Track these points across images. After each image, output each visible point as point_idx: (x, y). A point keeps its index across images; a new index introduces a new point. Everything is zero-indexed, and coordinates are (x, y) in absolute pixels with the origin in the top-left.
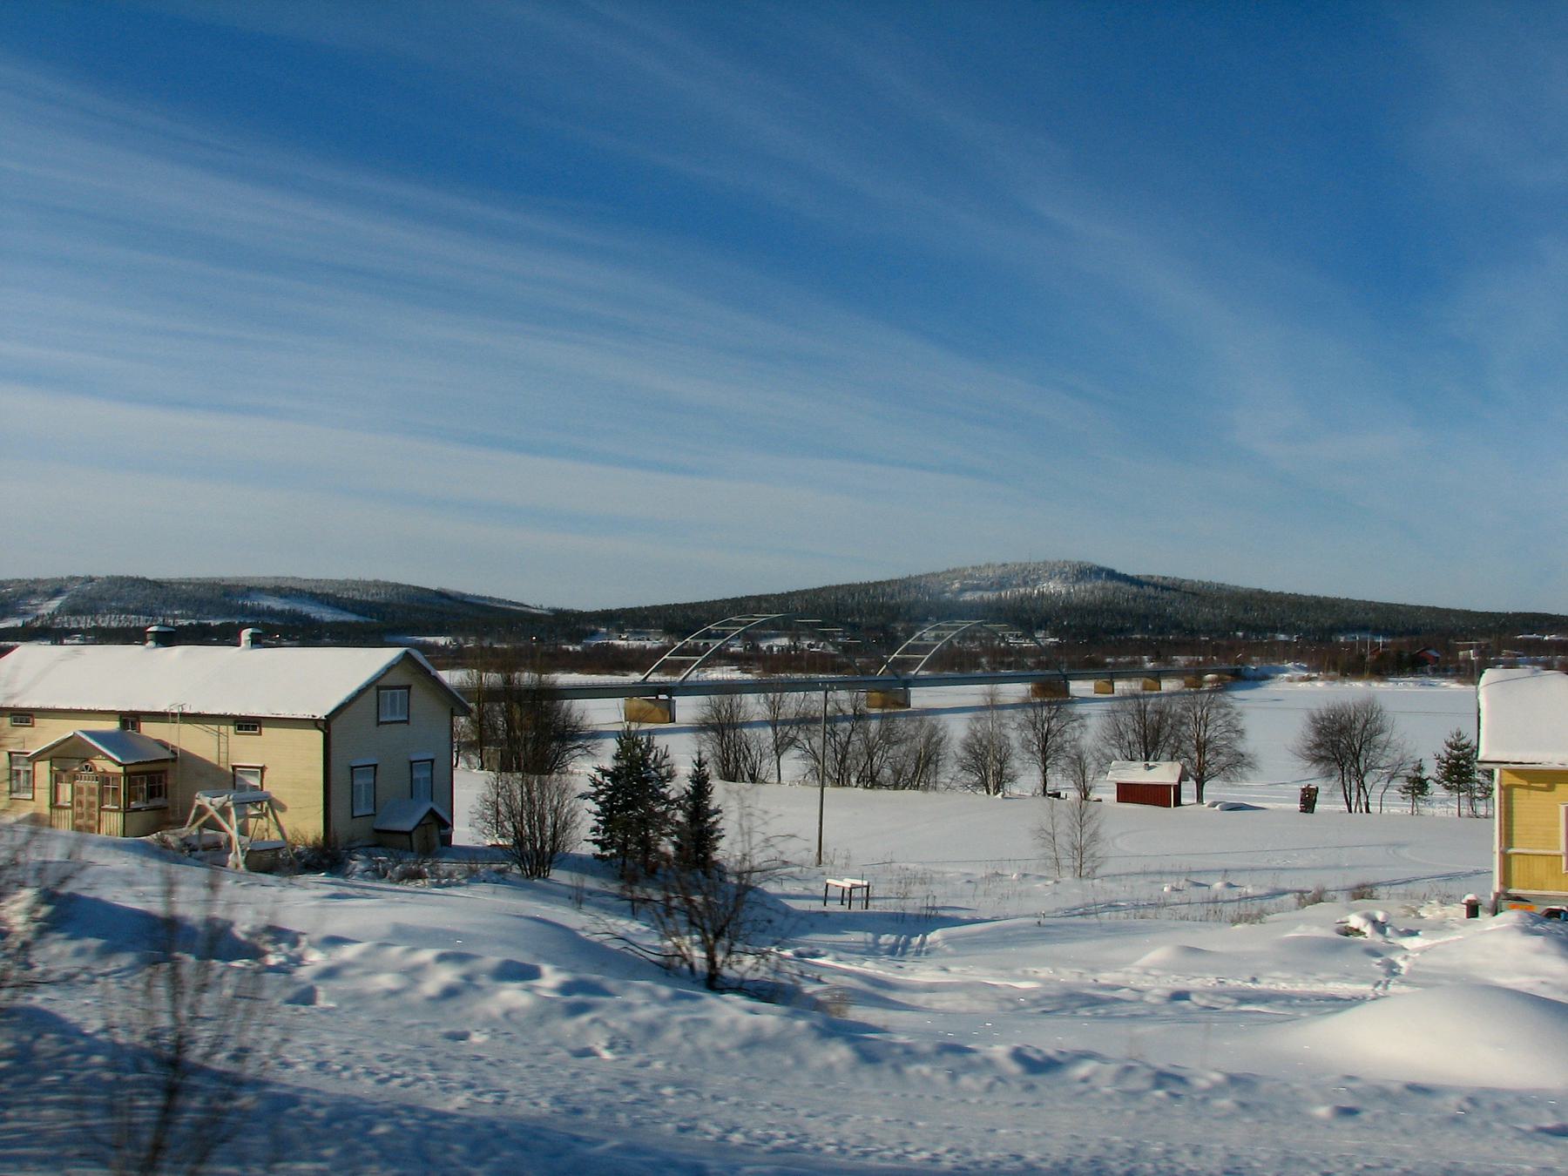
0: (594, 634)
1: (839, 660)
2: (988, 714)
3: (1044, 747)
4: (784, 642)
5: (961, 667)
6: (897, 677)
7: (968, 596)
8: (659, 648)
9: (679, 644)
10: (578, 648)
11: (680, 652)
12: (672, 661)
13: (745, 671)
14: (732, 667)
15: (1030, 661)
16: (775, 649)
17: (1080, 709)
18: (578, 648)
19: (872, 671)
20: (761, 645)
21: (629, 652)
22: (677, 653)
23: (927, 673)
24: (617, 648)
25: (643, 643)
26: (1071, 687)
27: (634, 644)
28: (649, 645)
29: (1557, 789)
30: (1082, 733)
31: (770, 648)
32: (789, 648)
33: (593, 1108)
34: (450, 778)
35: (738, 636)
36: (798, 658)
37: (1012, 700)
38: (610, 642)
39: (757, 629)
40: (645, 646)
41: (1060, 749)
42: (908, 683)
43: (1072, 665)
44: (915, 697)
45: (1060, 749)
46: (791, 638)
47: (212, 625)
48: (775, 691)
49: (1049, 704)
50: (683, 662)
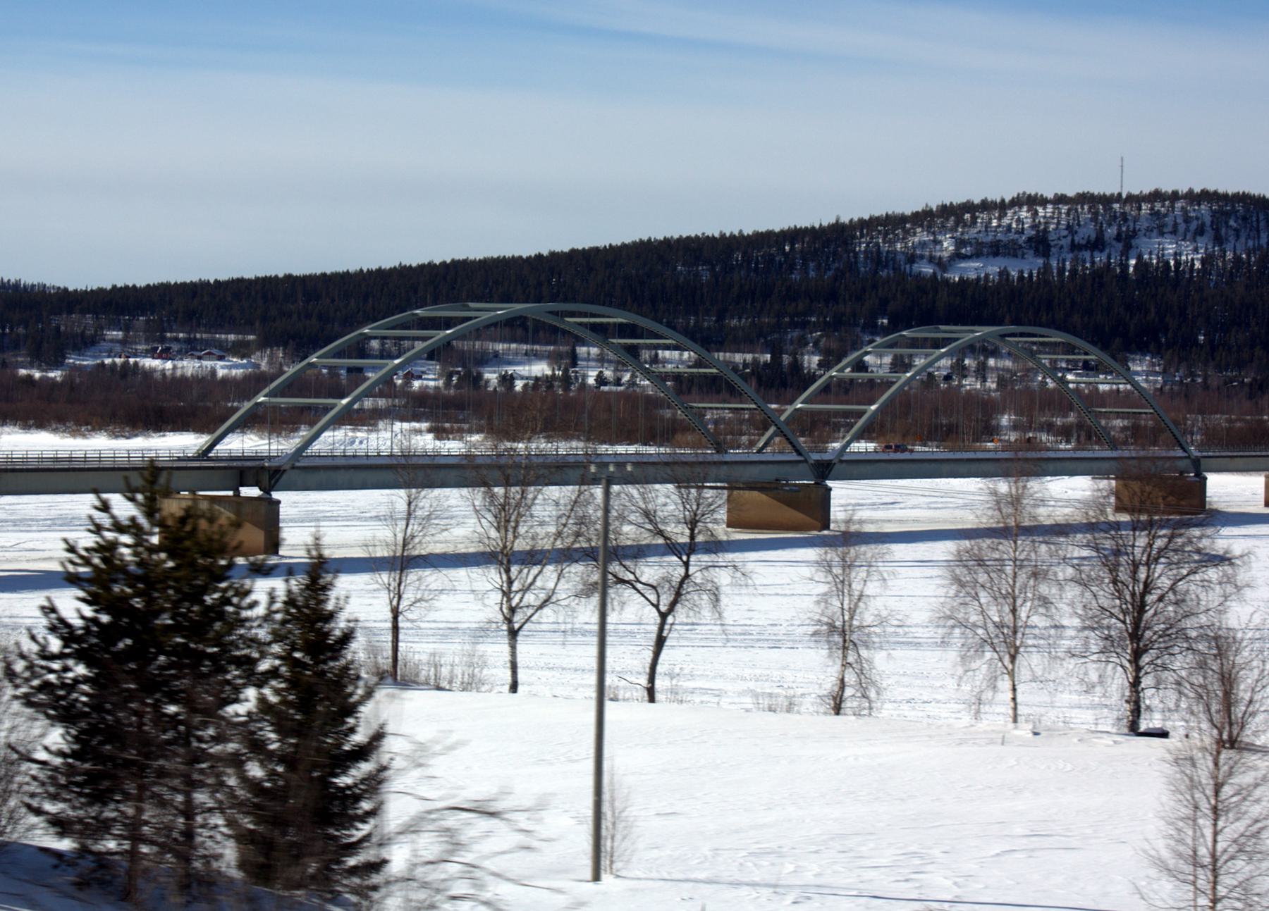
0: (86, 343)
1: (668, 414)
2: (1006, 546)
3: (1137, 623)
4: (540, 369)
5: (944, 434)
6: (799, 454)
7: (972, 269)
8: (246, 378)
9: (290, 370)
10: (55, 374)
11: (295, 387)
12: (275, 408)
13: (440, 433)
14: (416, 425)
15: (375, 344)
16: (519, 385)
17: (1227, 540)
18: (55, 374)
19: (744, 439)
20: (487, 376)
21: (179, 384)
22: (290, 388)
23: (871, 446)
24: (149, 373)
25: (208, 364)
26: (1209, 483)
27: (189, 366)
28: (223, 369)
29: (441, 260)
30: (1226, 598)
31: (507, 380)
32: (548, 381)
33: (809, 706)
34: (878, 465)
35: (432, 355)
36: (569, 406)
37: (1061, 514)
38: (132, 360)
39: (478, 338)
40: (213, 372)
41: (1174, 634)
42: (825, 470)
43: (1213, 439)
44: (386, 621)
45: (1174, 634)
46: (553, 358)
47: (221, 373)
48: (507, 483)
49: (1149, 525)
50: (309, 408)
